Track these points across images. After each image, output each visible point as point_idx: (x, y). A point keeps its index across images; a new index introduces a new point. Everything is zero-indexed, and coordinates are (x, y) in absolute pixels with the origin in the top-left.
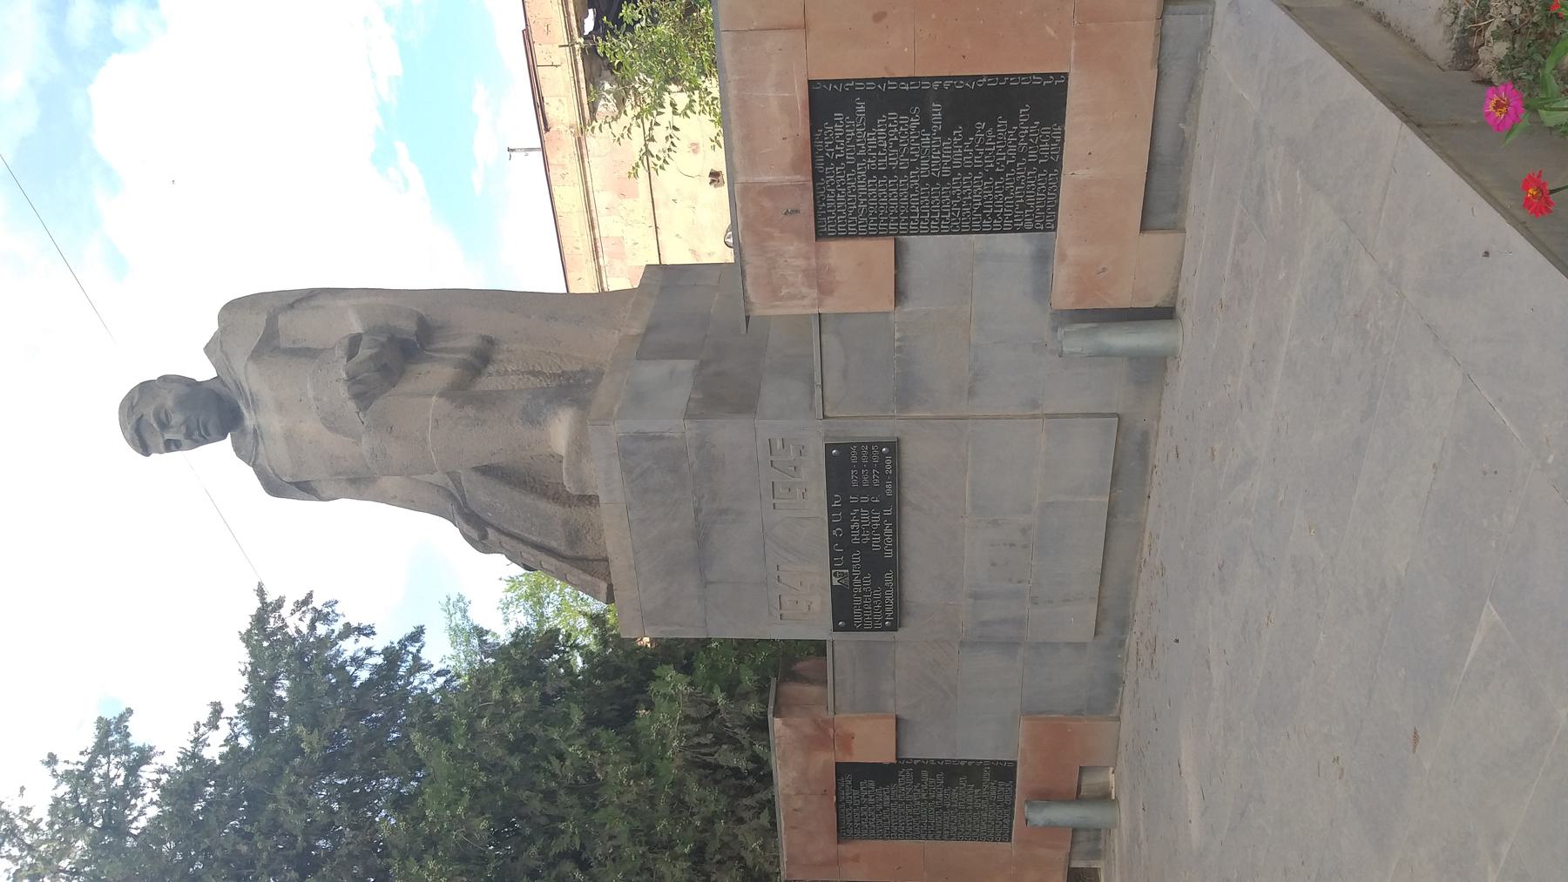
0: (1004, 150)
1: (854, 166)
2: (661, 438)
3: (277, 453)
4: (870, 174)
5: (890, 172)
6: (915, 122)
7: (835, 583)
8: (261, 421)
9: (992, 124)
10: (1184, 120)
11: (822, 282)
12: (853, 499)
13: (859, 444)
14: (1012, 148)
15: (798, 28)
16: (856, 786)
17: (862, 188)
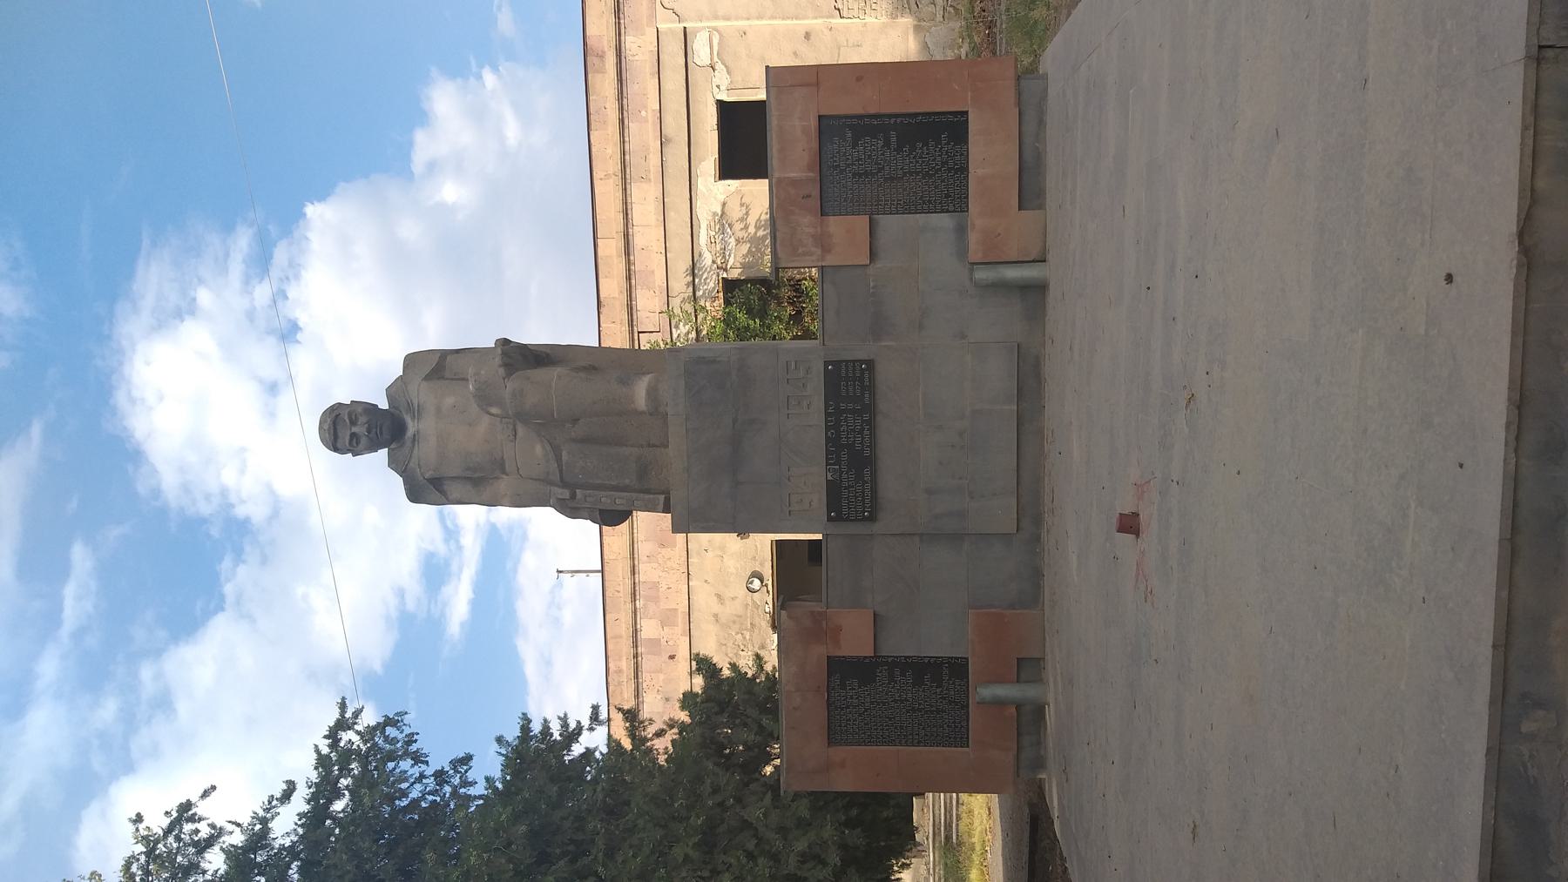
2: (714, 361)
3: (425, 454)
5: (866, 174)
6: (881, 143)
12: (843, 406)
13: (847, 361)
16: (843, 686)
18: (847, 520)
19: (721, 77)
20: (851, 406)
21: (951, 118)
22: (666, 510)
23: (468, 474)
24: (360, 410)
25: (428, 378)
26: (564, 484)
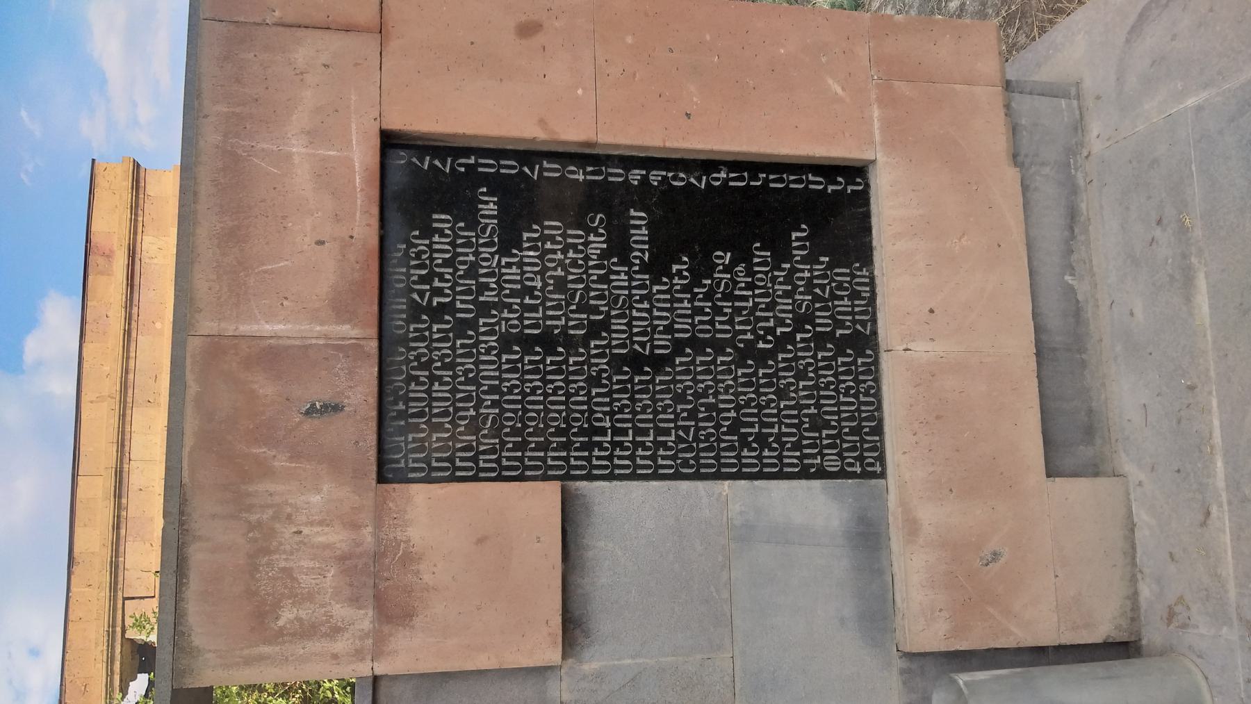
0: (771, 307)
1: (473, 324)
4: (506, 343)
5: (548, 341)
6: (598, 243)
9: (743, 256)
10: (1071, 269)
11: (386, 588)
14: (785, 304)
15: (368, 30)
17: (489, 371)
21: (817, 183)
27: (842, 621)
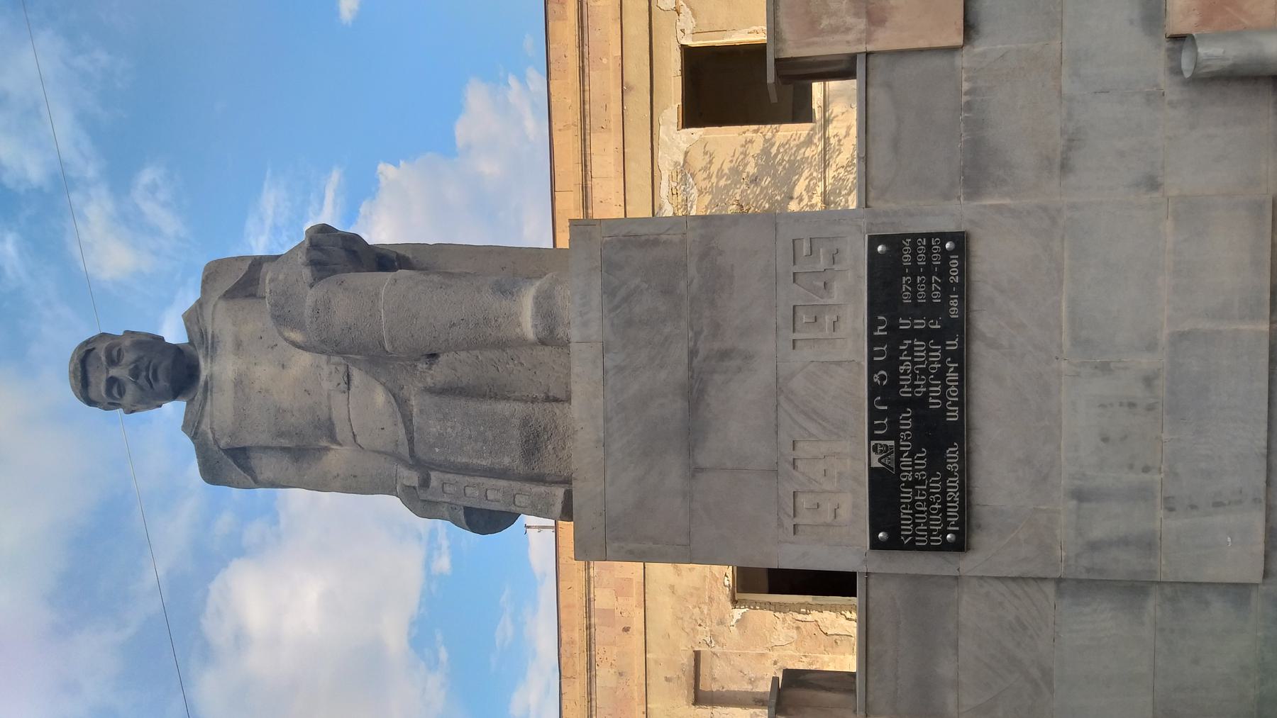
2: (655, 243)
7: (876, 464)
8: (216, 368)
12: (905, 325)
13: (915, 237)
18: (912, 547)
19: (686, 21)
20: (920, 324)
22: (567, 514)
23: (285, 442)
24: (127, 342)
25: (230, 295)
26: (416, 462)
27: (1131, 23)
